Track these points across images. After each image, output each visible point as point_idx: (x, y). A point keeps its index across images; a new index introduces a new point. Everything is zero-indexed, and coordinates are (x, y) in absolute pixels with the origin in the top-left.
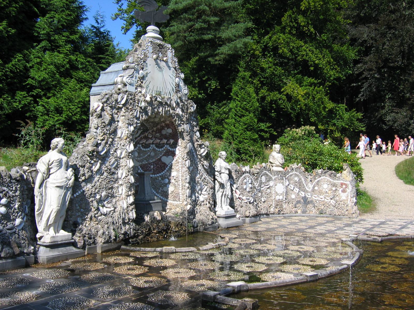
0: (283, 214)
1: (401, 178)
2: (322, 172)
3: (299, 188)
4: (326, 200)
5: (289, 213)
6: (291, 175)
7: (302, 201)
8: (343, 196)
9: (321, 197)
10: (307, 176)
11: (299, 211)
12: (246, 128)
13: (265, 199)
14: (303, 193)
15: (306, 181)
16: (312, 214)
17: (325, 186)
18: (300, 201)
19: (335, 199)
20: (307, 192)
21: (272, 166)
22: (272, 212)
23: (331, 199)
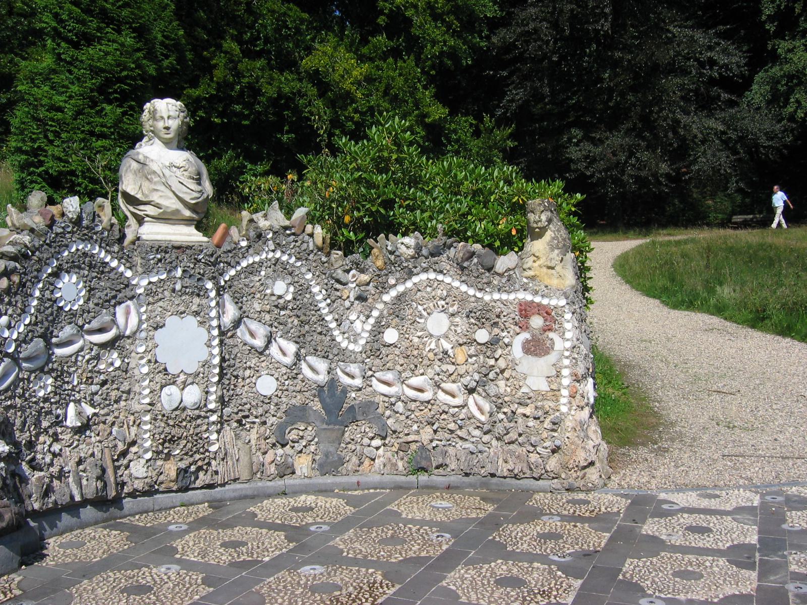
0: (210, 486)
1: (650, 292)
2: (418, 248)
3: (299, 340)
4: (441, 396)
5: (245, 475)
6: (252, 270)
7: (317, 405)
8: (535, 374)
9: (416, 381)
10: (340, 274)
11: (303, 465)
12: (101, 89)
13: (89, 411)
14: (322, 365)
15: (333, 298)
16: (372, 474)
17: (438, 323)
18: (304, 407)
19: (492, 389)
20: (343, 356)
21: (140, 221)
22: (138, 485)
23: (471, 391)
